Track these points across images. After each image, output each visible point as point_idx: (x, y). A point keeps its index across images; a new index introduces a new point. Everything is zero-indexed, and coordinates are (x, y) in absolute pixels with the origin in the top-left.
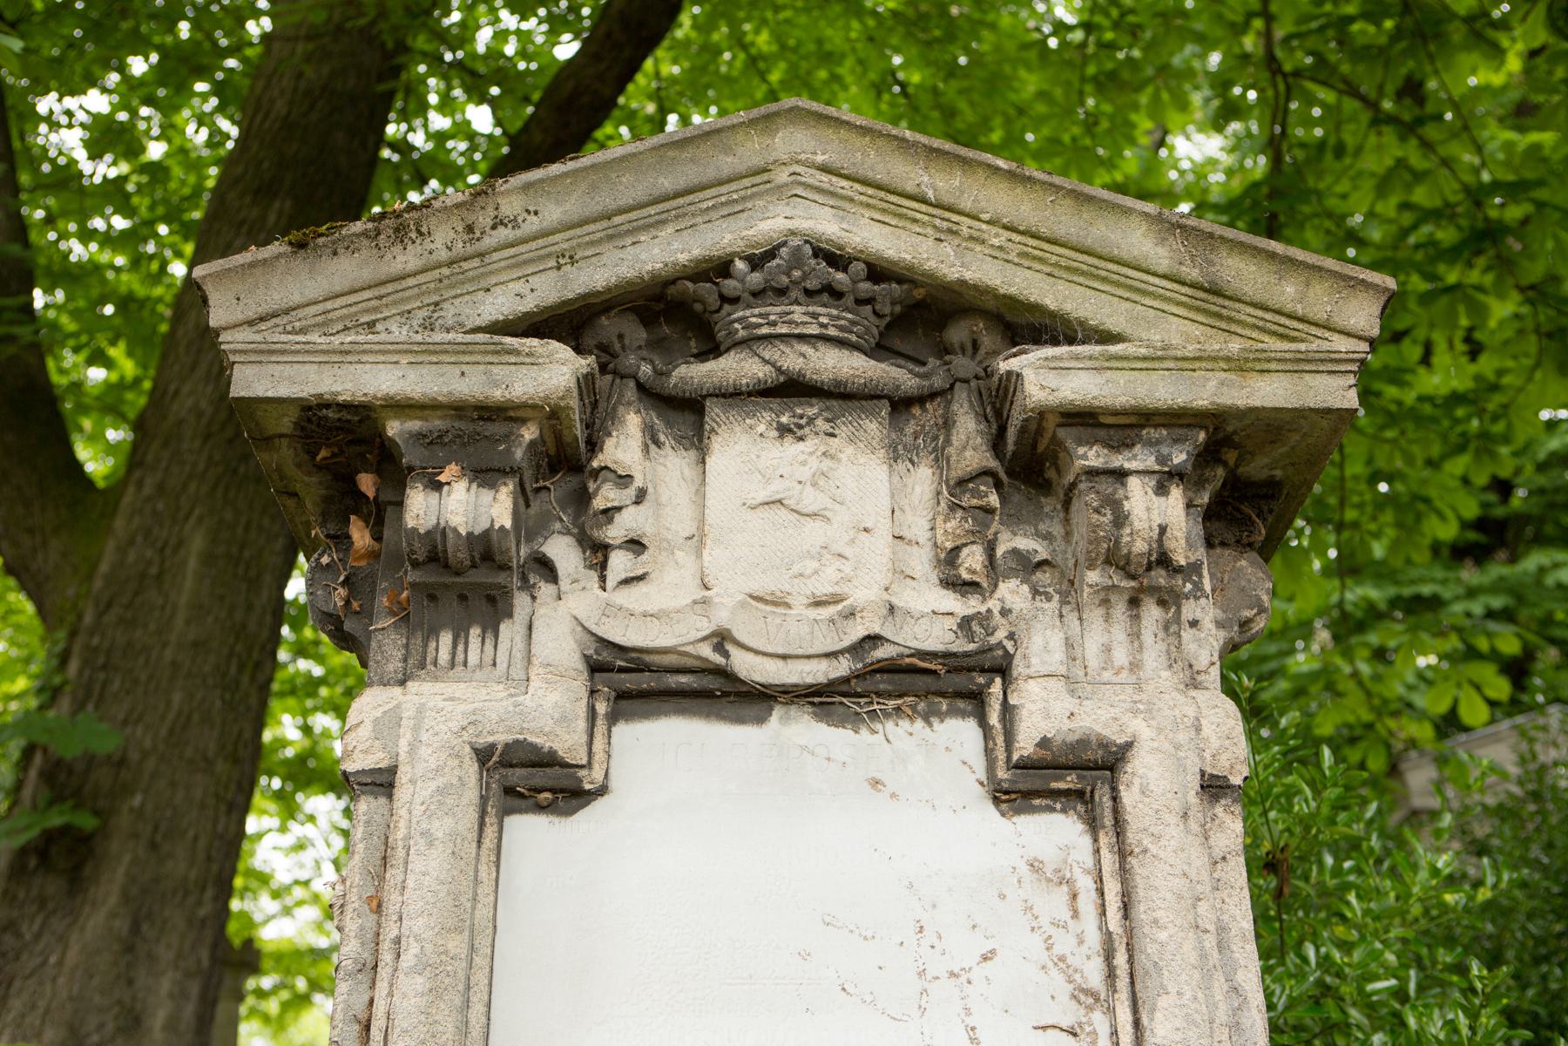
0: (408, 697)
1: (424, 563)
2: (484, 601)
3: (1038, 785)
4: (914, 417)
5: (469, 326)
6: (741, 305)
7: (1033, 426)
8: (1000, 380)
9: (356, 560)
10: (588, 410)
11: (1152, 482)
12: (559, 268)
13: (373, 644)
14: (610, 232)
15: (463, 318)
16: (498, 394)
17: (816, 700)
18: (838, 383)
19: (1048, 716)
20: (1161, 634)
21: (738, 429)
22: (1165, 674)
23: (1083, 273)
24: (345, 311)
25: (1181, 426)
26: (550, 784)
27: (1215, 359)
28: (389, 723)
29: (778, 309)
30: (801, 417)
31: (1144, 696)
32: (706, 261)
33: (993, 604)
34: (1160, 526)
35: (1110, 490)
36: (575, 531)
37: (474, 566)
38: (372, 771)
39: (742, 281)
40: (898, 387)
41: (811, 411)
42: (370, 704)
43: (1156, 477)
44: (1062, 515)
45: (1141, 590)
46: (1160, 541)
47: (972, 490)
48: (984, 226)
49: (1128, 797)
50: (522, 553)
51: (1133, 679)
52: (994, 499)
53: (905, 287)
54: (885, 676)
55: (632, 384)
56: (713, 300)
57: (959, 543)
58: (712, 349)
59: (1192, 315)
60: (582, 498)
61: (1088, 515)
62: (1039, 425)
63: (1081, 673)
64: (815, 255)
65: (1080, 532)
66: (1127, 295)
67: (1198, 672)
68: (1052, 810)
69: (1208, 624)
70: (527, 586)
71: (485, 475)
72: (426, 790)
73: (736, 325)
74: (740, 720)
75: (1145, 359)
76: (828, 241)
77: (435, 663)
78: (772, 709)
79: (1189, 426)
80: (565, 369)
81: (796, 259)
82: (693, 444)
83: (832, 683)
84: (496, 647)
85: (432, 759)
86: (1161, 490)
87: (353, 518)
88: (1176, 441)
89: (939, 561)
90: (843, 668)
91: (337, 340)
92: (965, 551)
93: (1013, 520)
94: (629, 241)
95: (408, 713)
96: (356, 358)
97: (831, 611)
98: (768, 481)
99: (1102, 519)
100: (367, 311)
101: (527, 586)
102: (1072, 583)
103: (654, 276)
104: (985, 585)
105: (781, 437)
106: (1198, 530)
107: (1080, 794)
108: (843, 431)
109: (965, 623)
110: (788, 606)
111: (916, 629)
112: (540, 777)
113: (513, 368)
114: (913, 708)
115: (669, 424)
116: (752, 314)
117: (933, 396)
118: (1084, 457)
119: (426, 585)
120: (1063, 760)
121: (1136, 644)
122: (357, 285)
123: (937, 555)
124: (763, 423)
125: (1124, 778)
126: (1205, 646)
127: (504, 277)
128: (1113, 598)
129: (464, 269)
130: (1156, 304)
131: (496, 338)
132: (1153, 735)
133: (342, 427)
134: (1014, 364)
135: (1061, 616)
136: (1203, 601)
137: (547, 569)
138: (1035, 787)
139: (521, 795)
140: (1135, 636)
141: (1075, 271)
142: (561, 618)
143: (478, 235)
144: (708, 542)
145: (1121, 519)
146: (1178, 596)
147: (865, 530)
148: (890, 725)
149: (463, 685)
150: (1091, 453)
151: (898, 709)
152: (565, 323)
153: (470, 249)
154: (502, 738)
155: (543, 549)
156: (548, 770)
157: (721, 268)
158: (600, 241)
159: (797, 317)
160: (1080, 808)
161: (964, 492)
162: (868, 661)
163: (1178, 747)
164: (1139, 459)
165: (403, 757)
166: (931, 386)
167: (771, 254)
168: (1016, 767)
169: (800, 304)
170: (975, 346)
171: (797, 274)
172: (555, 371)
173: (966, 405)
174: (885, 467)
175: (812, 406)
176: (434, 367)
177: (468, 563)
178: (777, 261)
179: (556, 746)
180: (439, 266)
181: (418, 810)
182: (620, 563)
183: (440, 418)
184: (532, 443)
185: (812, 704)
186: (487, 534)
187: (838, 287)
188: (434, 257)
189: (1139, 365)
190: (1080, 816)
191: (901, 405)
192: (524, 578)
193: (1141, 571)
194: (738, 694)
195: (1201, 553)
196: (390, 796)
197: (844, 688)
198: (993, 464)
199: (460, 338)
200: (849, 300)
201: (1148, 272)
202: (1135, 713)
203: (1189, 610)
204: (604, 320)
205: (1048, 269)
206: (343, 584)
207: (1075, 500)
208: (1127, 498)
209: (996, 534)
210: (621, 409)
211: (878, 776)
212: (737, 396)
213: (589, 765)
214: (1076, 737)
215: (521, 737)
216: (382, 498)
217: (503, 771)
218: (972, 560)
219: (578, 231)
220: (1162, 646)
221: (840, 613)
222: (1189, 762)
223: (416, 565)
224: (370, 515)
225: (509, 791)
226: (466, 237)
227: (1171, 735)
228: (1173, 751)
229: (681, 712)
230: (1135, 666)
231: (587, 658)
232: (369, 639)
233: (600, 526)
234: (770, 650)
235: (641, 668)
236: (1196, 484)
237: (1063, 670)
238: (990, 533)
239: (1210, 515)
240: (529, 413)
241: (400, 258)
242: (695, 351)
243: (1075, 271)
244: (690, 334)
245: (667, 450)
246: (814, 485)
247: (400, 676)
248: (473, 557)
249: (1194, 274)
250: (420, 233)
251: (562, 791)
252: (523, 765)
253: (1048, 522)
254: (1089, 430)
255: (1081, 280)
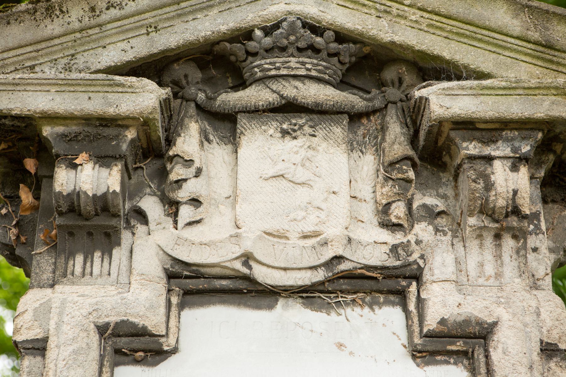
0: (56, 295)
1: (66, 213)
2: (103, 236)
3: (439, 347)
4: (363, 125)
5: (93, 69)
6: (259, 57)
7: (435, 130)
8: (415, 102)
9: (23, 211)
10: (167, 121)
11: (509, 163)
12: (148, 34)
13: (34, 263)
14: (179, 12)
15: (89, 64)
16: (111, 111)
17: (304, 295)
18: (317, 104)
19: (445, 306)
20: (515, 256)
21: (257, 132)
22: (518, 280)
23: (467, 37)
24: (15, 59)
25: (527, 129)
26: (143, 346)
27: (548, 88)
28: (44, 310)
29: (281, 60)
30: (295, 125)
31: (504, 294)
32: (238, 30)
33: (411, 238)
34: (513, 190)
35: (482, 169)
36: (159, 193)
37: (97, 215)
38: (33, 341)
39: (260, 43)
40: (354, 106)
41: (301, 121)
42: (31, 300)
43: (511, 160)
44: (453, 184)
45: (502, 229)
46: (514, 199)
47: (398, 169)
48: (406, 8)
49: (495, 356)
50: (126, 207)
51: (497, 283)
52: (411, 174)
53: (358, 46)
54: (346, 281)
55: (193, 105)
56: (242, 54)
57: (390, 200)
58: (241, 84)
59: (534, 61)
60: (163, 174)
61: (469, 183)
62: (439, 129)
63: (465, 279)
64: (304, 27)
65: (464, 194)
66: (494, 49)
67: (538, 280)
68: (448, 363)
69: (544, 249)
70: (129, 226)
71: (104, 159)
72: (66, 351)
73: (256, 69)
74: (258, 307)
75: (504, 88)
76: (311, 18)
77: (73, 274)
78: (277, 301)
79: (532, 129)
80: (152, 95)
81: (292, 29)
82: (230, 141)
83: (314, 285)
84: (110, 264)
85: (70, 333)
86: (514, 168)
87: (21, 185)
88: (524, 138)
89: (378, 211)
90: (320, 275)
91: (10, 77)
92: (394, 206)
93: (423, 186)
94: (190, 17)
95: (55, 304)
96: (22, 88)
97: (313, 241)
98: (275, 163)
99: (478, 186)
100: (30, 59)
101: (129, 226)
102: (459, 224)
103: (206, 39)
104: (406, 226)
105: (283, 137)
106: (538, 193)
107: (465, 354)
108: (320, 133)
109: (394, 249)
110: (287, 238)
111: (364, 252)
112: (137, 343)
113: (121, 95)
114: (363, 300)
115: (215, 129)
116: (265, 63)
117: (374, 112)
118: (467, 148)
119: (67, 226)
120: (454, 332)
121: (499, 262)
122: (23, 43)
123: (377, 207)
124: (272, 128)
125: (492, 344)
126: (542, 263)
127: (114, 39)
128: (485, 234)
129: (90, 33)
130: (512, 55)
131: (110, 77)
132: (510, 318)
133: (14, 130)
134: (424, 92)
135: (453, 245)
136: (541, 236)
137: (141, 216)
138: (437, 349)
139: (125, 354)
140: (498, 257)
141: (462, 35)
142: (150, 246)
143: (98, 13)
144: (239, 200)
145: (489, 186)
146: (525, 233)
147: (334, 193)
148: (349, 310)
149: (90, 287)
150: (471, 146)
151: (354, 301)
152: (152, 67)
153: (93, 22)
154: (113, 319)
155: (139, 204)
156: (142, 338)
157: (246, 35)
158: (173, 18)
159: (293, 65)
160: (466, 362)
161: (393, 170)
162: (336, 271)
163: (526, 325)
164: (501, 149)
165: (52, 332)
166: (374, 106)
167: (277, 26)
168: (426, 336)
169: (294, 56)
170: (401, 81)
171: (292, 38)
172: (145, 97)
173: (395, 117)
174: (346, 155)
175: (302, 118)
176: (72, 94)
177: (93, 213)
178: (280, 30)
179: (147, 324)
180: (74, 32)
181: (61, 364)
182: (186, 213)
183: (76, 125)
184: (132, 141)
185: (302, 297)
186: (105, 195)
187: (318, 46)
188: (71, 26)
189: (501, 92)
190: (465, 367)
191: (355, 117)
192: (128, 222)
193: (501, 217)
194: (257, 292)
195: (539, 207)
196: (44, 356)
197: (321, 288)
198: (411, 152)
199: (88, 76)
200: (324, 54)
201: (507, 35)
202: (499, 304)
203: (532, 241)
204: (176, 66)
205: (445, 34)
206: (15, 226)
207: (461, 175)
208: (493, 173)
209: (413, 195)
210: (186, 120)
211: (342, 341)
212: (256, 112)
213: (167, 335)
214: (462, 318)
215: (125, 318)
216: (40, 173)
217: (114, 339)
218: (398, 211)
219: (160, 12)
220: (515, 264)
221: (318, 243)
222: (533, 335)
223: (61, 214)
224: (32, 184)
225: (117, 351)
226: (90, 14)
227: (521, 318)
228: (522, 327)
229: (223, 302)
230: (498, 275)
231: (166, 270)
232: (31, 259)
233: (174, 190)
234: (276, 265)
235: (198, 276)
236: (536, 165)
237: (454, 277)
238: (409, 195)
239: (545, 184)
240: (130, 122)
241: (49, 27)
242: (231, 85)
243: (462, 35)
244: (228, 75)
245: (215, 144)
246: (303, 165)
247: (51, 282)
248: (96, 209)
249: (535, 35)
250: (62, 12)
251: (150, 351)
252: (127, 336)
253: (444, 188)
254: (470, 132)
255: (465, 40)
